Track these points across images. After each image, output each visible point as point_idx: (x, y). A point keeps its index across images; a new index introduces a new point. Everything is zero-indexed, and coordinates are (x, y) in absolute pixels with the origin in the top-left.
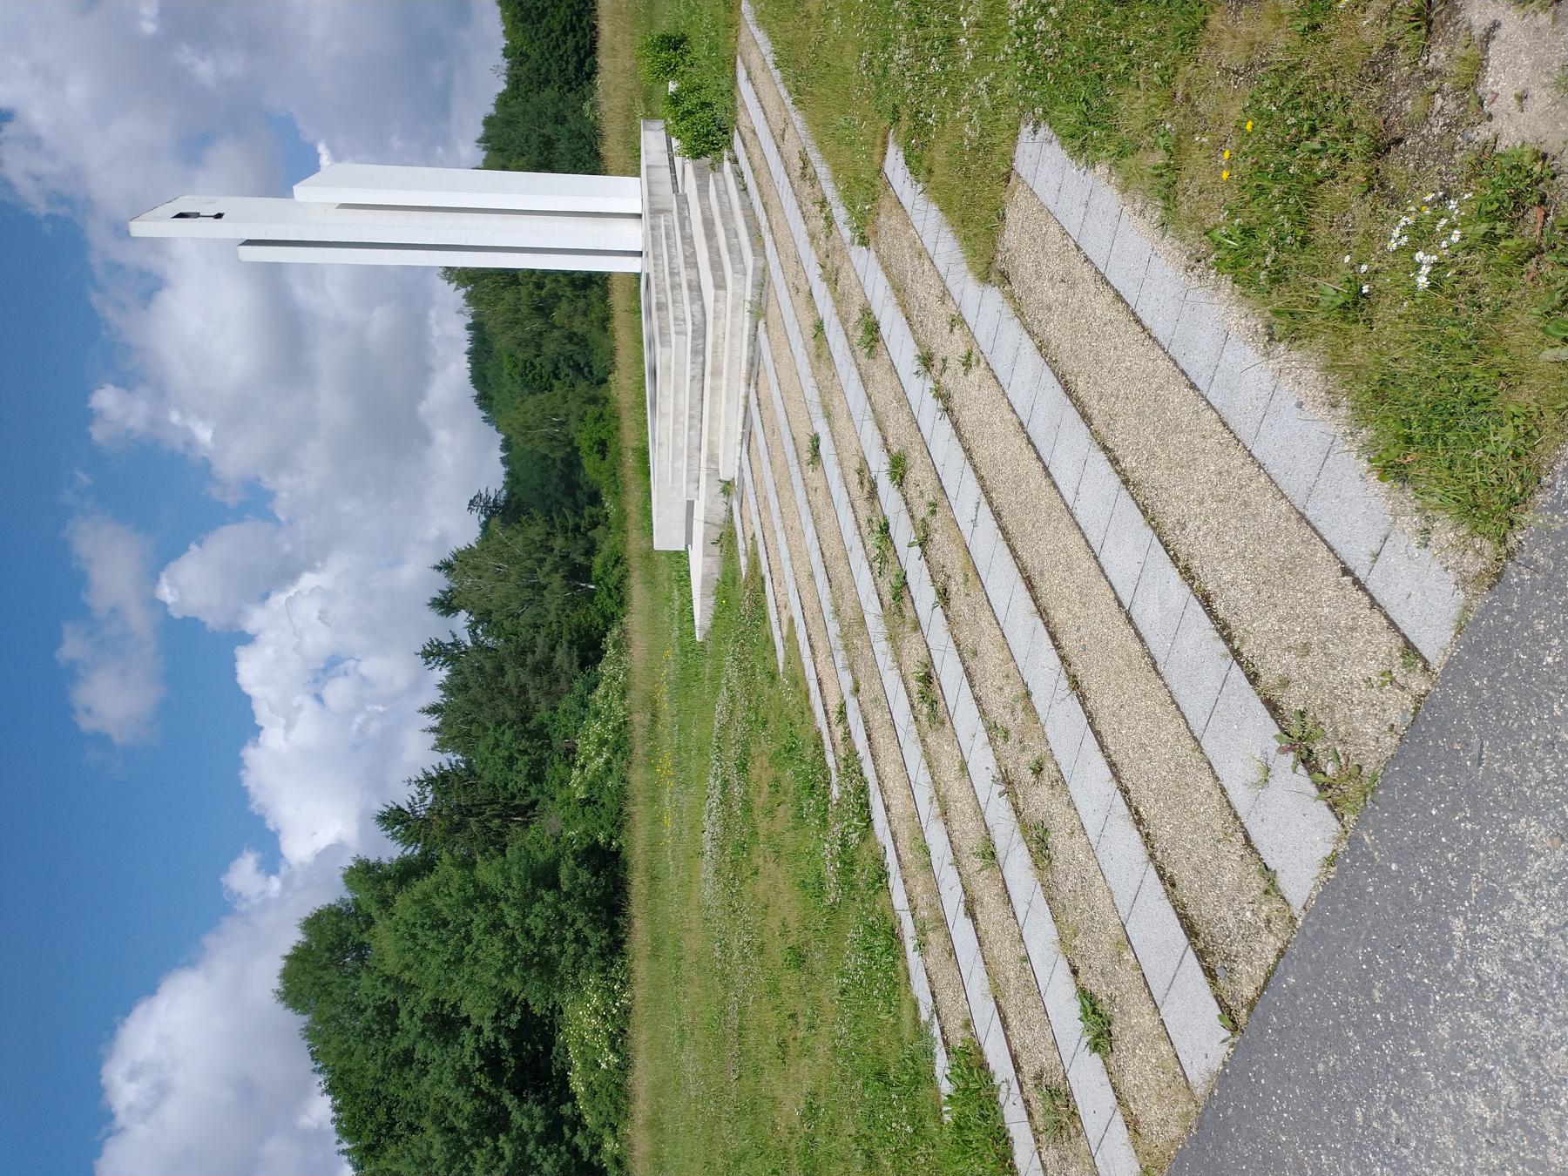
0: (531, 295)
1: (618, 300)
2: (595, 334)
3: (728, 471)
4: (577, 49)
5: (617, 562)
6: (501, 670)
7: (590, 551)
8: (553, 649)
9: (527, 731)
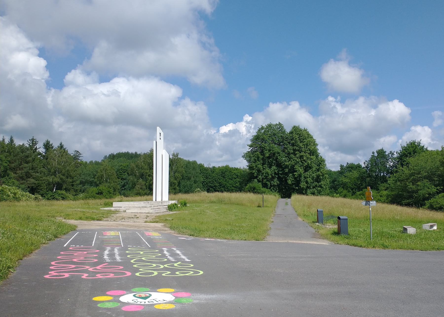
0: (147, 173)
1: (149, 197)
2: (135, 191)
3: (127, 211)
4: (215, 186)
5: (63, 198)
6: (27, 162)
7: (67, 190)
8: (34, 178)
9: (7, 170)
